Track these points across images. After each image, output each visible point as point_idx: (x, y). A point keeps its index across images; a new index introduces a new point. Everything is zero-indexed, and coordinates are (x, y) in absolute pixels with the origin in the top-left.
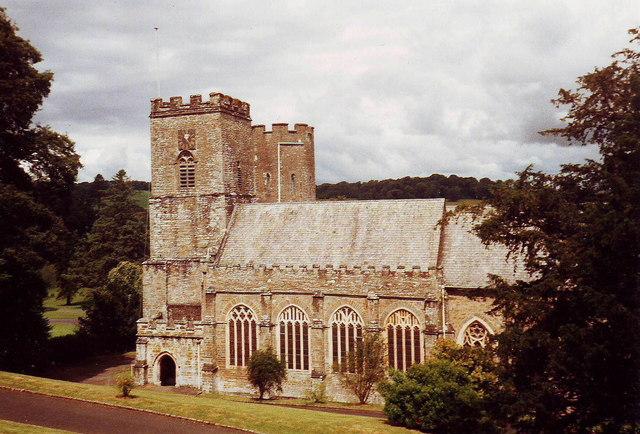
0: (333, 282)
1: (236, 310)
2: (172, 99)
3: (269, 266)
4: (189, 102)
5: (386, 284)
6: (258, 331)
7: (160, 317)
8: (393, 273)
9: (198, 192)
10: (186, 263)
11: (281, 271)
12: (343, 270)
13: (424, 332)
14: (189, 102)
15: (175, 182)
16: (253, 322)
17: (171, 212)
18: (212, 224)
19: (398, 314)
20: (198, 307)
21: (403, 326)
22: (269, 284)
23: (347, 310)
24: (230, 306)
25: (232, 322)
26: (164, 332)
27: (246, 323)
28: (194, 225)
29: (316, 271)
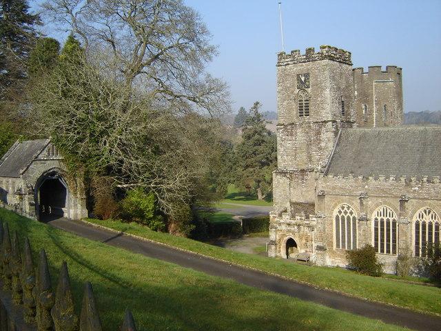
0: (417, 188)
7: (285, 211)
15: (295, 112)
17: (292, 135)
18: (323, 144)
23: (427, 211)
26: (288, 221)
28: (309, 145)
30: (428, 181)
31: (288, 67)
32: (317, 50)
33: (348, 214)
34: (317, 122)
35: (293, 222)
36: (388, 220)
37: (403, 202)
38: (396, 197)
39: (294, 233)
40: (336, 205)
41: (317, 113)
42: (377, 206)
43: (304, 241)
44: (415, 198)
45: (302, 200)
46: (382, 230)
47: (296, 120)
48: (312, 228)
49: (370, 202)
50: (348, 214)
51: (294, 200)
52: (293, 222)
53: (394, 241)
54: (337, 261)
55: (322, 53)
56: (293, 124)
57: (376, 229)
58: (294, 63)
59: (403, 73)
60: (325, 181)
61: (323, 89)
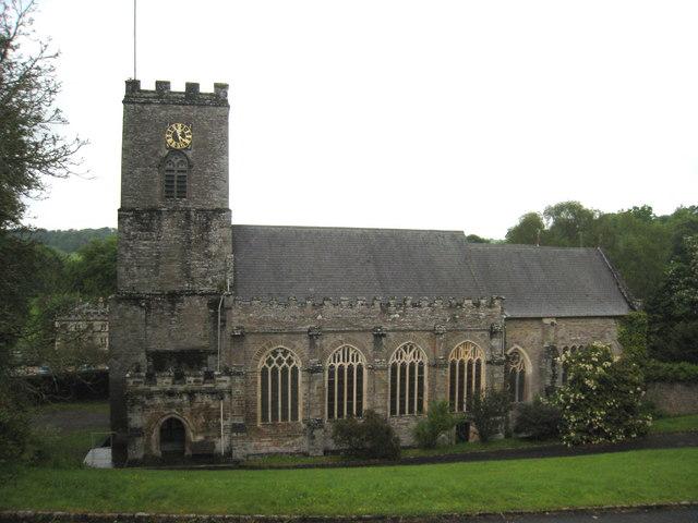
5: (454, 319)
10: (174, 297)
13: (488, 363)
16: (295, 369)
17: (149, 229)
18: (213, 249)
30: (414, 305)
31: (147, 108)
33: (275, 364)
35: (181, 388)
36: (351, 367)
37: (379, 336)
39: (180, 407)
40: (264, 350)
42: (334, 346)
44: (393, 331)
45: (170, 346)
46: (341, 382)
47: (160, 203)
49: (326, 342)
50: (275, 364)
51: (153, 347)
52: (181, 388)
54: (265, 444)
57: (331, 383)
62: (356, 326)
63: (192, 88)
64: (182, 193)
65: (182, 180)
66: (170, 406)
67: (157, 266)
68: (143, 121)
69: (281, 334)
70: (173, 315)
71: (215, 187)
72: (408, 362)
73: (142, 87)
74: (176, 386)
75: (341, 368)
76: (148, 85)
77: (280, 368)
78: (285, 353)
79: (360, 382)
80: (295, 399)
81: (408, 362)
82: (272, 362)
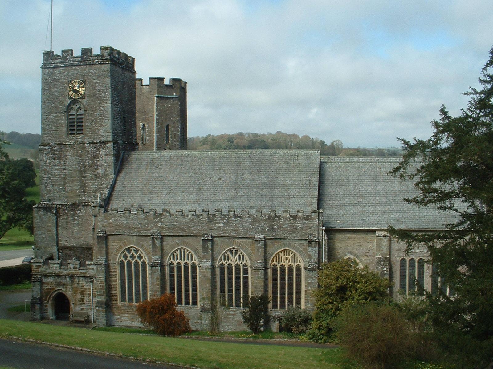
0: (222, 225)
1: (126, 252)
2: (63, 51)
3: (159, 211)
4: (80, 54)
5: (272, 229)
6: (148, 271)
7: (51, 258)
8: (279, 217)
9: (87, 140)
11: (171, 215)
12: (231, 214)
14: (80, 54)
16: (144, 263)
17: (60, 158)
18: (101, 171)
19: (281, 254)
20: (89, 249)
21: (286, 265)
22: (160, 227)
23: (234, 251)
24: (121, 247)
25: (122, 262)
26: (58, 271)
27: (136, 263)
29: (205, 215)
31: (57, 71)
32: (96, 51)
33: (129, 258)
34: (93, 143)
35: (65, 272)
38: (196, 236)
39: (64, 285)
40: (121, 247)
41: (94, 131)
43: (79, 296)
46: (179, 276)
48: (90, 279)
53: (266, 279)
55: (103, 56)
56: (61, 144)
58: (66, 66)
59: (143, 81)
60: (107, 218)
61: (102, 101)
62: (189, 233)
63: (86, 52)
64: (80, 130)
65: (80, 121)
66: (58, 284)
67: (65, 184)
68: (54, 80)
69: (133, 236)
70: (74, 220)
71: (102, 125)
72: (234, 265)
73: (55, 54)
74: (61, 270)
75: (237, 267)
76: (58, 52)
77: (133, 262)
78: (137, 251)
79: (299, 280)
80: (145, 287)
81: (234, 265)
82: (138, 257)
